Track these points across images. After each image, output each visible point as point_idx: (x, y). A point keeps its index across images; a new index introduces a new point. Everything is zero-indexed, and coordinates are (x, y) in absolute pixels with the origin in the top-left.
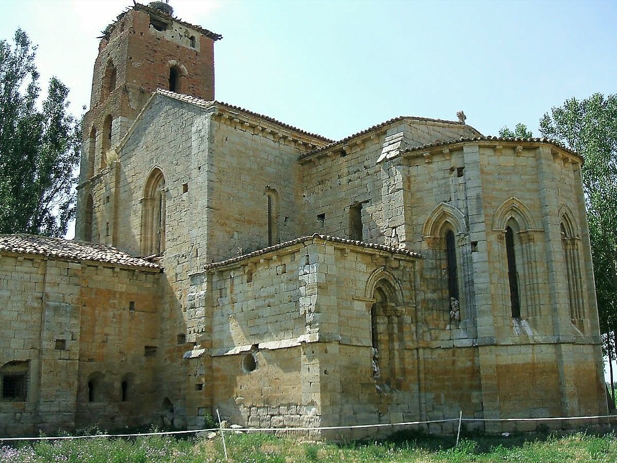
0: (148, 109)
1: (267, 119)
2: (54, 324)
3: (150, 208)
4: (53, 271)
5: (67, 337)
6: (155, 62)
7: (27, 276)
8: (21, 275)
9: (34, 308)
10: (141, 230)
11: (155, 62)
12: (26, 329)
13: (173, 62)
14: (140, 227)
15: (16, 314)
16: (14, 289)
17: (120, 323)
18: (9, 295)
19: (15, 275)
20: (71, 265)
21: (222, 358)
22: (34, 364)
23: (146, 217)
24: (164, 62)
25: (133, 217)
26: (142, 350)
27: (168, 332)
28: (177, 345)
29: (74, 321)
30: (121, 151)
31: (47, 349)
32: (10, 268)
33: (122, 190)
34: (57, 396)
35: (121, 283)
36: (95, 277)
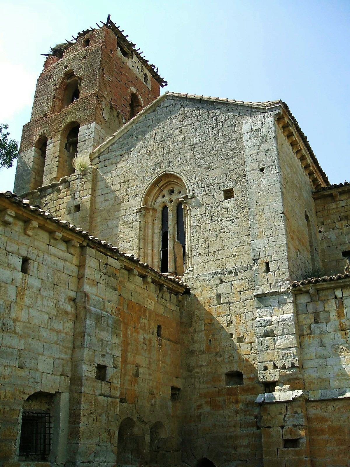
0: (149, 112)
1: (304, 139)
2: (96, 340)
3: (150, 219)
4: (93, 262)
5: (108, 362)
6: (121, 82)
7: (60, 264)
8: (55, 260)
9: (66, 313)
10: (139, 244)
11: (121, 82)
12: (56, 343)
13: (133, 89)
14: (138, 240)
15: (46, 317)
16: (45, 279)
17: (150, 351)
18: (39, 286)
19: (48, 258)
20: (111, 261)
21: (337, 403)
22: (65, 397)
23: (145, 230)
24: (127, 88)
25: (122, 229)
26: (168, 392)
27: (204, 370)
28: (224, 386)
29: (116, 340)
30: (98, 157)
31: (88, 377)
32: (44, 247)
33: (99, 199)
34: (96, 454)
35: (150, 299)
36: (127, 284)
